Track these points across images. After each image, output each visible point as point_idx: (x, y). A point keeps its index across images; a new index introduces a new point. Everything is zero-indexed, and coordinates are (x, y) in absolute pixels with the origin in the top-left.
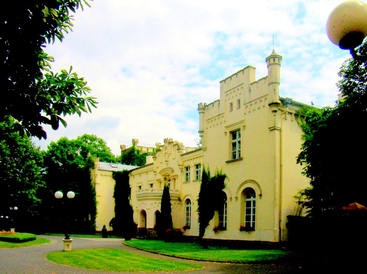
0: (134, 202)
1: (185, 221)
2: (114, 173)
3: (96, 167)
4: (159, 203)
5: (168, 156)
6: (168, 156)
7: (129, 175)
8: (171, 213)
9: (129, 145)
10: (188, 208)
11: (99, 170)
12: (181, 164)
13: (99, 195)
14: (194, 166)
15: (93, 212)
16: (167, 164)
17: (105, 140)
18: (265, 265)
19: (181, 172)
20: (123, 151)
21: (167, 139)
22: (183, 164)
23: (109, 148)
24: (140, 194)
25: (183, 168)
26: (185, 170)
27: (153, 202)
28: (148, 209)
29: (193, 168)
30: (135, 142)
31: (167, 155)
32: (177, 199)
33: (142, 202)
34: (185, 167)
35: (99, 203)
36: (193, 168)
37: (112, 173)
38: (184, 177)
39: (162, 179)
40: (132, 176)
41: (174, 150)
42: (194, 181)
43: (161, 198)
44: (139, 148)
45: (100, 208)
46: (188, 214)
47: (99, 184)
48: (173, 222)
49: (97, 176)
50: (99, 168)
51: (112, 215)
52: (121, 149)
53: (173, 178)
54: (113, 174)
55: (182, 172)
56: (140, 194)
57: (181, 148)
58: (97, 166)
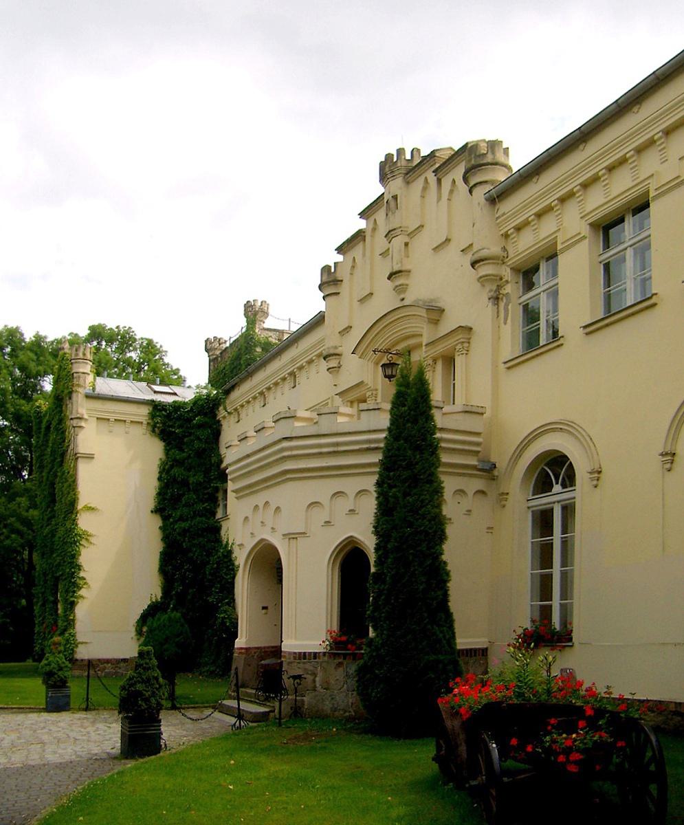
0: (243, 525)
1: (576, 573)
2: (156, 407)
3: (79, 385)
4: (361, 492)
5: (406, 244)
6: (406, 244)
7: (221, 413)
8: (446, 547)
9: (231, 328)
10: (543, 521)
11: (88, 396)
12: (495, 250)
13: (93, 506)
14: (585, 230)
15: (64, 577)
16: (400, 289)
17: (159, 340)
18: (585, 744)
19: (489, 308)
20: (216, 359)
21: (400, 152)
22: (504, 249)
23: (178, 370)
24: (248, 456)
25: (506, 273)
26: (512, 288)
27: (322, 489)
28: (291, 537)
29: (584, 245)
30: (255, 314)
31: (398, 242)
32: (473, 461)
33: (259, 499)
34: (515, 270)
35: (92, 540)
36: (584, 245)
37: (145, 410)
38: (510, 338)
39: (369, 380)
40: (229, 413)
41: (439, 199)
42: (591, 329)
43: (377, 458)
44: (270, 334)
45: (96, 563)
46: (544, 556)
47: (90, 457)
48: (454, 605)
49: (83, 424)
50: (94, 389)
51: (149, 588)
52: (206, 353)
53: (440, 349)
54: (152, 416)
55: (496, 299)
56: (248, 456)
57: (489, 158)
58: (81, 382)
